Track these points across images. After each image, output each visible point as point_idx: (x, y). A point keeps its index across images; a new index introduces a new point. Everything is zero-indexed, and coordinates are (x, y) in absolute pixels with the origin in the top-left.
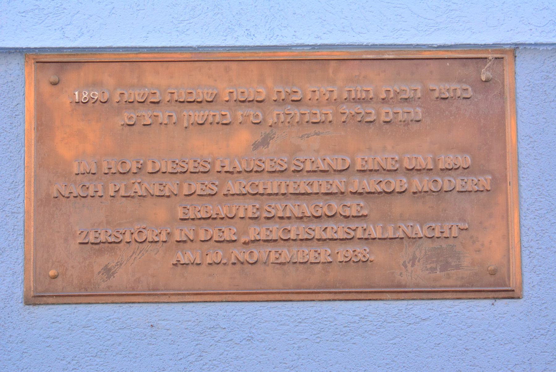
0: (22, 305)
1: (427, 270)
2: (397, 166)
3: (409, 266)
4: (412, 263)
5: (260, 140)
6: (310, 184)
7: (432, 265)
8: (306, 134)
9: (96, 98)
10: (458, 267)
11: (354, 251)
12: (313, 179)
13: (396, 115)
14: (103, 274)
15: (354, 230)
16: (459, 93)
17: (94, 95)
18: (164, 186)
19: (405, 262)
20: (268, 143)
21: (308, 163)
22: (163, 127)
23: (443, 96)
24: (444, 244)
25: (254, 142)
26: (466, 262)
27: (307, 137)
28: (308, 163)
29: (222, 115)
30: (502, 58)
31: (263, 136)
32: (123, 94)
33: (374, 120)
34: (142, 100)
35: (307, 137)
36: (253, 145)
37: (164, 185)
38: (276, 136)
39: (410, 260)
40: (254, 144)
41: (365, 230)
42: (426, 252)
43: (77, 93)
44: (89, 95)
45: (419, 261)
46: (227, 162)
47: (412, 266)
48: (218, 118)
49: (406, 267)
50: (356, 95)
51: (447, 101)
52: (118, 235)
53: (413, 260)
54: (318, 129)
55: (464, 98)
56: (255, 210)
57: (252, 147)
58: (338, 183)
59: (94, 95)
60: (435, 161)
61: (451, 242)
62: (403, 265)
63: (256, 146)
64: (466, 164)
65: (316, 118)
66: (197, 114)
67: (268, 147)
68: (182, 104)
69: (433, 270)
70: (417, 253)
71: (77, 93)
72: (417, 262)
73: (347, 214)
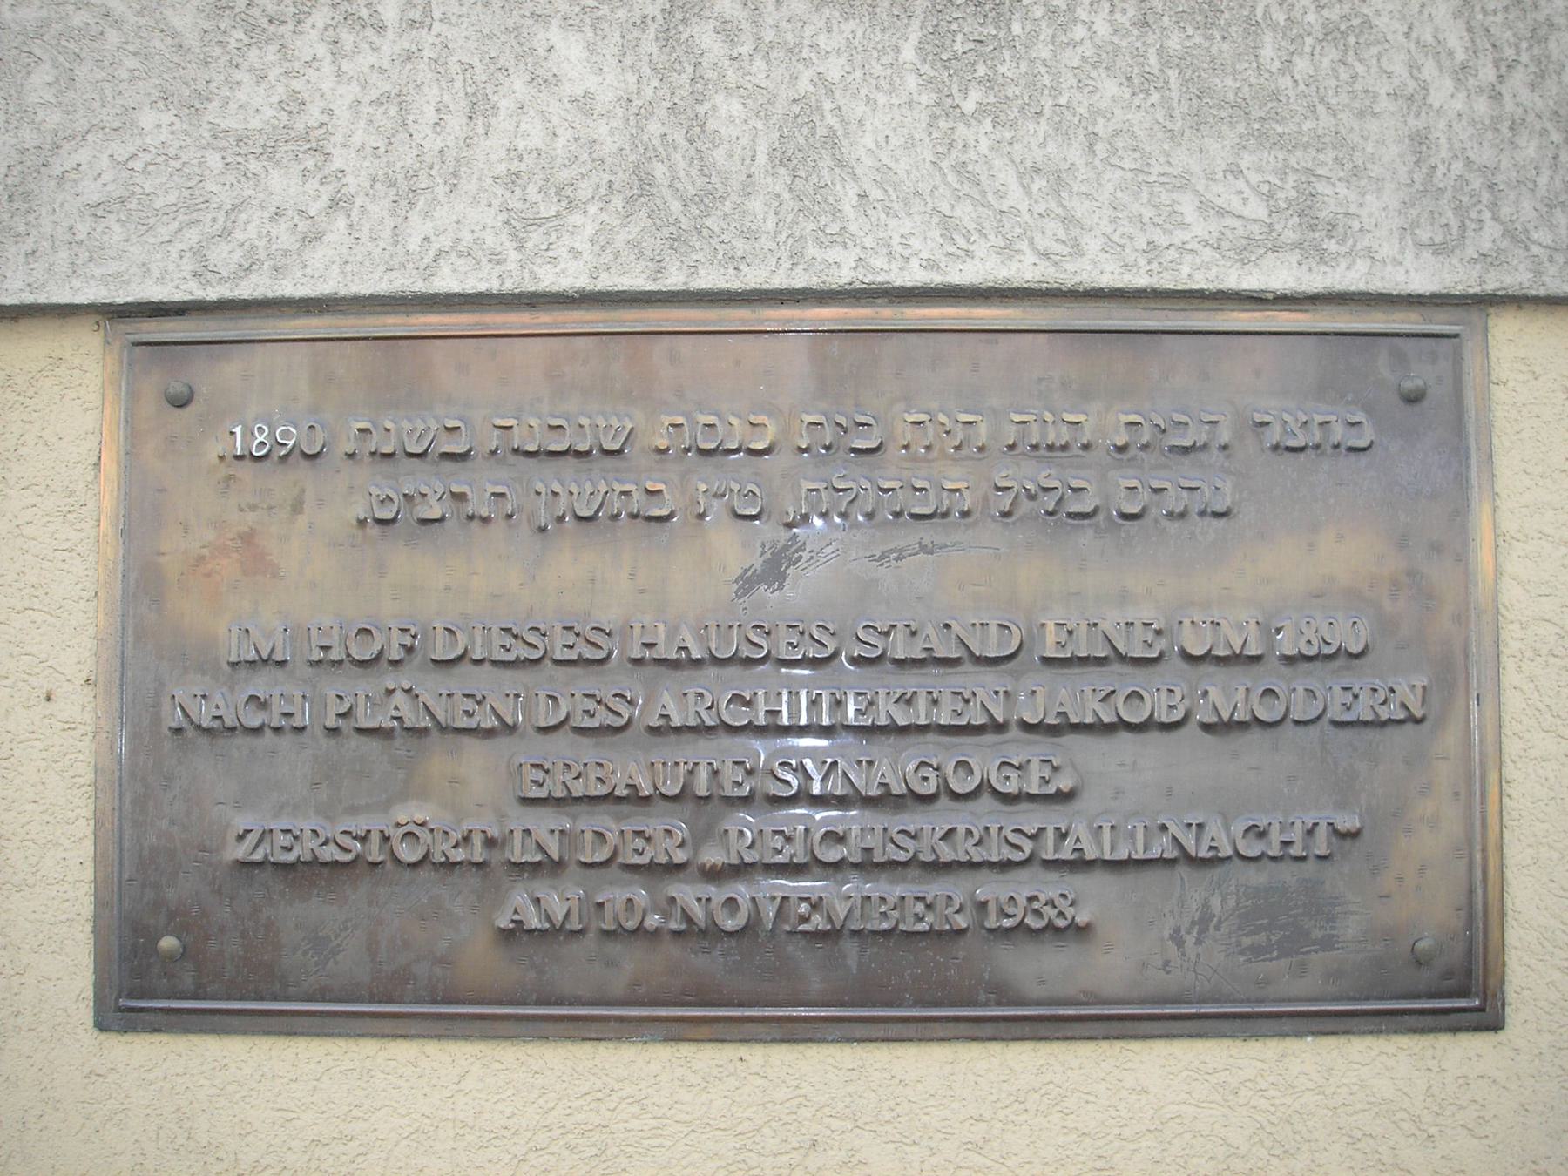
0: (88, 1035)
1: (1242, 953)
2: (1160, 645)
3: (1190, 940)
4: (1199, 933)
5: (758, 566)
6: (907, 701)
7: (1255, 938)
8: (892, 551)
9: (291, 443)
10: (1328, 944)
11: (1031, 899)
12: (910, 681)
13: (1156, 497)
14: (305, 953)
15: (1033, 837)
16: (1338, 433)
17: (286, 434)
18: (967, 701)
19: (1177, 930)
20: (782, 577)
21: (899, 636)
22: (475, 524)
23: (1292, 443)
24: (1288, 874)
25: (740, 572)
26: (1350, 928)
27: (896, 559)
28: (899, 636)
29: (648, 491)
30: (1456, 336)
31: (768, 555)
32: (502, 495)
33: (1096, 511)
34: (420, 450)
35: (896, 559)
36: (736, 581)
37: (479, 698)
38: (806, 555)
39: (1193, 923)
40: (741, 577)
41: (914, 633)
42: (1238, 902)
43: (238, 430)
44: (272, 434)
45: (1217, 928)
46: (661, 636)
47: (1198, 942)
48: (638, 502)
49: (1180, 943)
50: (1044, 435)
51: (1302, 456)
52: (346, 841)
53: (1204, 922)
54: (927, 533)
55: (1352, 449)
56: (1150, 637)
57: (735, 587)
58: (986, 693)
59: (286, 434)
60: (1269, 631)
61: (1310, 867)
62: (1171, 937)
63: (747, 583)
64: (1357, 642)
65: (926, 502)
66: (581, 489)
67: (781, 587)
68: (531, 461)
69: (1257, 951)
70: (1216, 902)
71: (238, 430)
72: (1212, 929)
73: (1011, 788)
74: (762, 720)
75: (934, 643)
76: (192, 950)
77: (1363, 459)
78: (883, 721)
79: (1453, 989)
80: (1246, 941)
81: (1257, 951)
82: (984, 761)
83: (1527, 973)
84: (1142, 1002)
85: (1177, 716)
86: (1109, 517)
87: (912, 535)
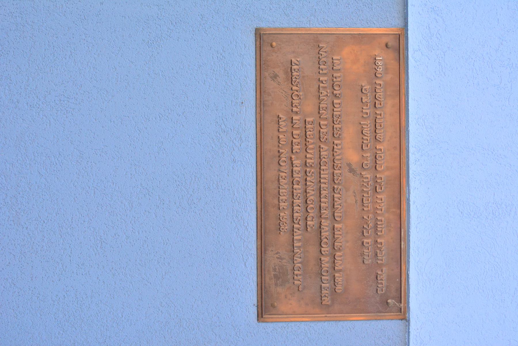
0: (255, 26)
3: (277, 256)
10: (276, 284)
15: (298, 223)
19: (279, 253)
20: (350, 172)
24: (290, 276)
26: (279, 289)
49: (277, 254)
53: (280, 258)
54: (359, 202)
61: (291, 280)
63: (349, 165)
65: (365, 201)
69: (275, 270)
70: (284, 261)
74: (322, 168)
75: (337, 203)
76: (260, 35)
77: (375, 292)
78: (322, 192)
79: (265, 309)
80: (277, 267)
81: (275, 270)
82: (312, 213)
83: (268, 327)
84: (264, 242)
85: (323, 253)
86: (362, 238)
87: (359, 199)
